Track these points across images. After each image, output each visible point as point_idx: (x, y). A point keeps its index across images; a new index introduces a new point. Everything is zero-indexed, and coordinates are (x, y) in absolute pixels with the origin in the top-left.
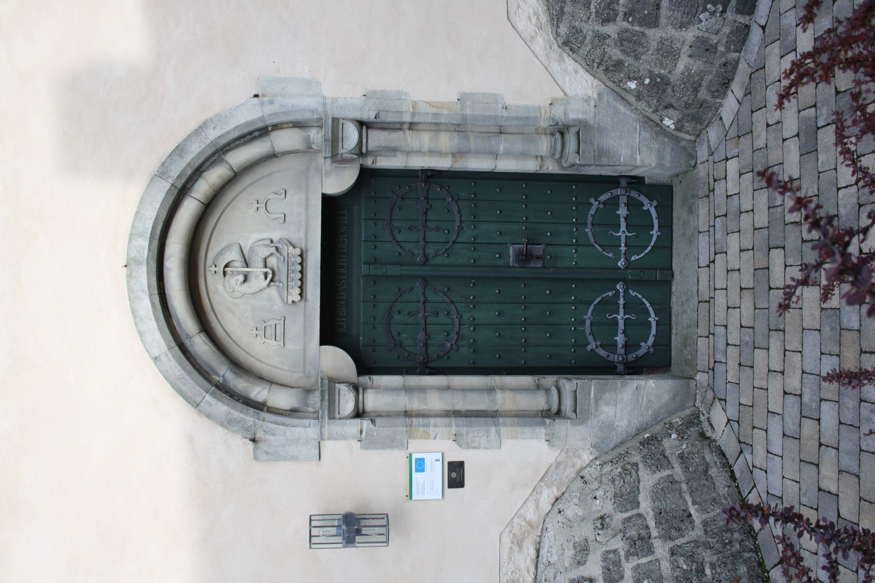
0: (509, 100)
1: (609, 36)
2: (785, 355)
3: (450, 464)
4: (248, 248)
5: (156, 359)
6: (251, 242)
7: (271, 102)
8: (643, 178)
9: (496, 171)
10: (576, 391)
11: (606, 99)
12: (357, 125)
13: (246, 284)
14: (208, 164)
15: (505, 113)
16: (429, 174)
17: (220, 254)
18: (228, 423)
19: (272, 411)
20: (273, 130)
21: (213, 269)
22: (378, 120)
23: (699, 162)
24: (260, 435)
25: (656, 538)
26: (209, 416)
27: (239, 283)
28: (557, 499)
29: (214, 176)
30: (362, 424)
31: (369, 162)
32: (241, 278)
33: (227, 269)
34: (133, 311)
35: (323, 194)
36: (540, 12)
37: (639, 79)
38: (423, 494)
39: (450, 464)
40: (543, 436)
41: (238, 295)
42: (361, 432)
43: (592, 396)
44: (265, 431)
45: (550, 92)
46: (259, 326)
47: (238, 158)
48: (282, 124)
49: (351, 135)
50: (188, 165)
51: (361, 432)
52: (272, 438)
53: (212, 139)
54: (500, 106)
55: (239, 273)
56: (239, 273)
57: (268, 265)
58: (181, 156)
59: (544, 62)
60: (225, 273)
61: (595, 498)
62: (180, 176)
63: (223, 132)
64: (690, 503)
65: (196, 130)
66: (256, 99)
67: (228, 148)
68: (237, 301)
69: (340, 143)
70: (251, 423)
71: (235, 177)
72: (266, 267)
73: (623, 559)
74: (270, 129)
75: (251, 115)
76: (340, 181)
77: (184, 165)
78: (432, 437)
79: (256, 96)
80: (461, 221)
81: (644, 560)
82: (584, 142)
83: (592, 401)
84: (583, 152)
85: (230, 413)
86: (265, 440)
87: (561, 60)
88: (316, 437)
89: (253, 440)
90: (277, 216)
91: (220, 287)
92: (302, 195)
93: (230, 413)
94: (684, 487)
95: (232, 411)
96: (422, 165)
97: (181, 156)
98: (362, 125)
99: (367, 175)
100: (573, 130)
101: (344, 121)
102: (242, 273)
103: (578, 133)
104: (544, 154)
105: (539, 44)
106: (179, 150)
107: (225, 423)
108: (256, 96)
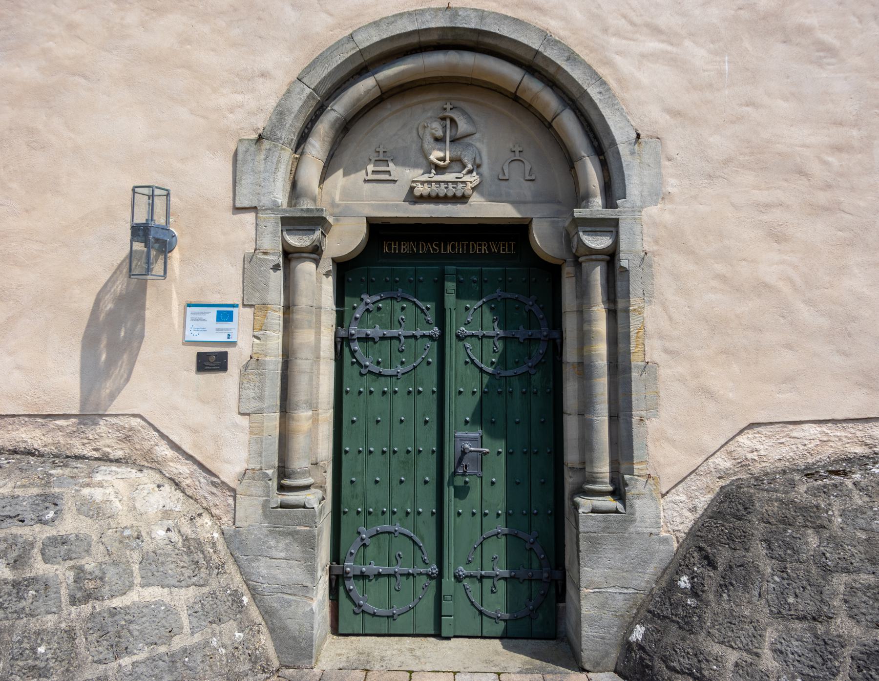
0: (652, 425)
1: (747, 550)
2: (667, 492)
3: (225, 354)
4: (470, 142)
5: (351, 37)
6: (478, 145)
7: (632, 153)
8: (564, 601)
9: (565, 416)
10: (304, 507)
11: (662, 548)
12: (611, 252)
13: (432, 140)
14: (562, 95)
15: (635, 420)
16: (558, 341)
17: (464, 113)
18: (280, 113)
19: (297, 163)
20: (601, 161)
21: (448, 106)
22: (618, 272)
23: (590, 675)
24: (266, 144)
25: (94, 608)
26: (288, 91)
27: (433, 131)
28: (177, 484)
29: (548, 101)
30: (274, 254)
31: (568, 270)
32: (439, 133)
33: (448, 122)
34: (401, 15)
35: (531, 220)
36: (764, 464)
37: (694, 592)
38: (192, 319)
39: (225, 354)
40: (251, 466)
41: (421, 132)
42: (265, 253)
43: (298, 528)
44: (270, 149)
45: (669, 474)
46: (388, 154)
47: (569, 124)
48: (608, 170)
49: (600, 242)
50: (559, 68)
51: (265, 253)
52: (262, 157)
53: (589, 91)
54: (643, 413)
55: (445, 132)
56: (445, 132)
57: (454, 164)
58: (568, 59)
59: (701, 468)
60: (443, 119)
61: (169, 530)
62: (546, 58)
63: (597, 101)
64: (135, 658)
65: (597, 74)
66: (635, 136)
67: (579, 114)
68: (415, 132)
69: (589, 229)
70: (279, 135)
71: (547, 125)
72: (451, 161)
73: (72, 563)
74: (602, 157)
75: (620, 131)
76: (543, 239)
77: (558, 62)
78: (255, 333)
79: (638, 136)
80: (506, 377)
81: (64, 592)
82: (605, 520)
83: (291, 528)
84: (593, 519)
85: (291, 113)
86: (260, 150)
87: (709, 489)
88: (261, 204)
89: (260, 137)
90: (506, 172)
91: (429, 114)
92: (529, 198)
93: (291, 113)
94: (162, 649)
95: (293, 115)
96: (568, 329)
97: (568, 59)
98: (611, 257)
99: (551, 273)
100: (620, 506)
101: (614, 233)
102: (445, 136)
103: (617, 511)
104: (587, 469)
105: (723, 462)
106: (572, 57)
107: (280, 109)
108: (638, 136)
